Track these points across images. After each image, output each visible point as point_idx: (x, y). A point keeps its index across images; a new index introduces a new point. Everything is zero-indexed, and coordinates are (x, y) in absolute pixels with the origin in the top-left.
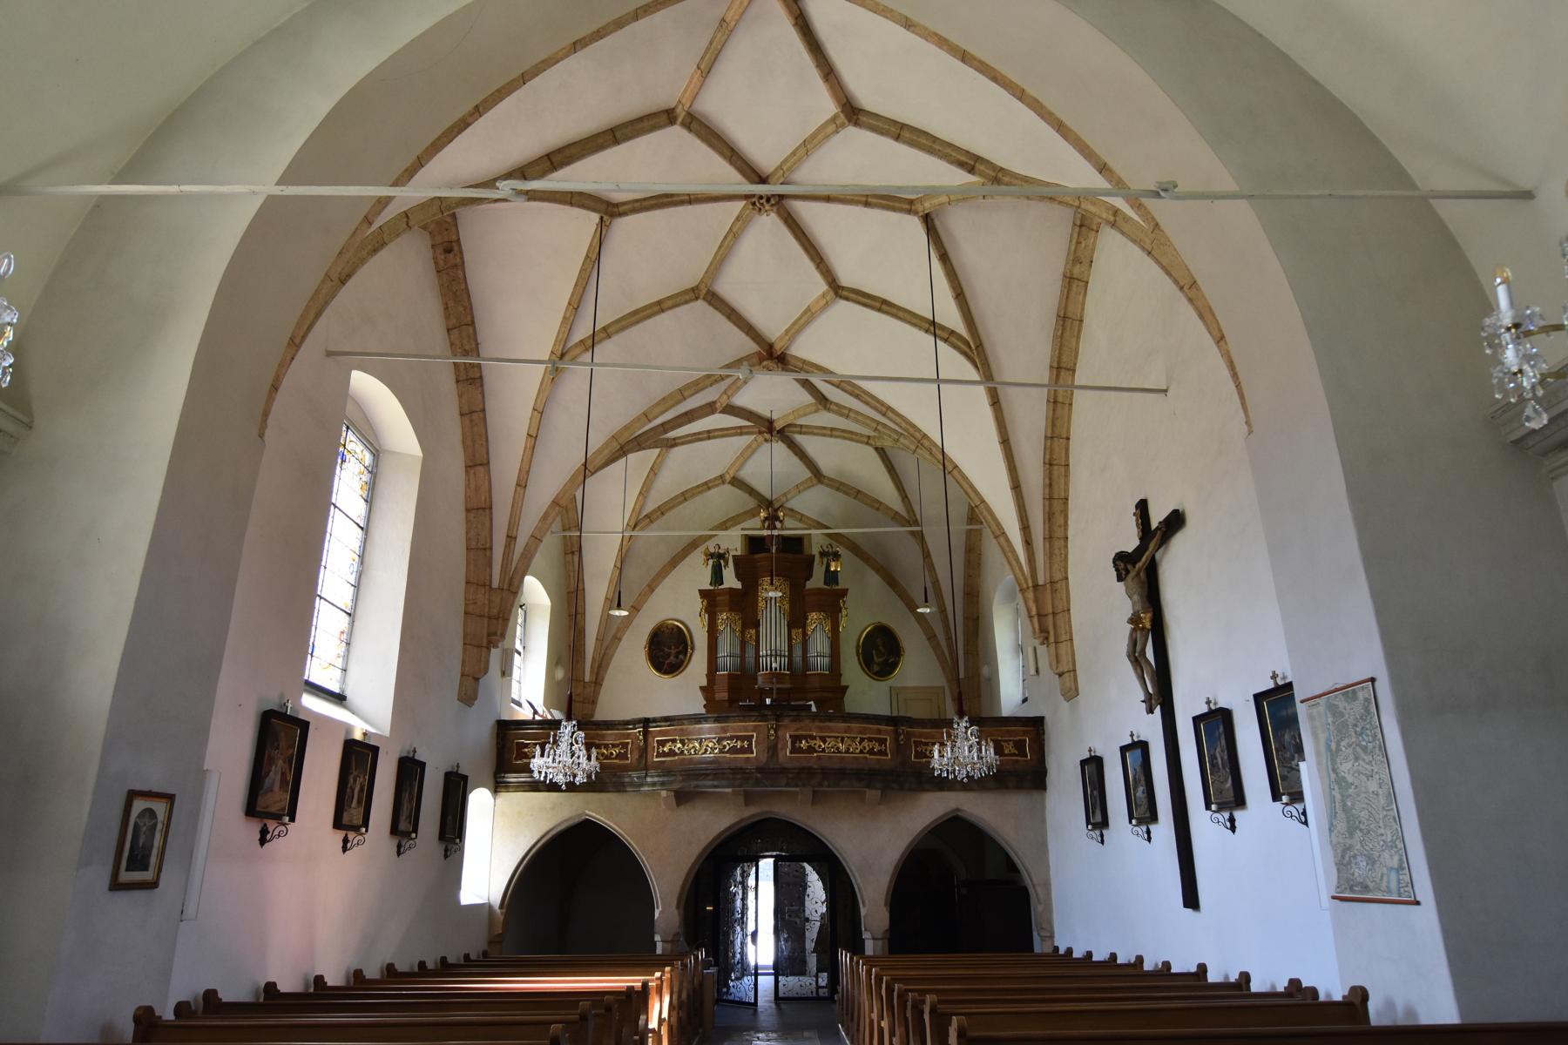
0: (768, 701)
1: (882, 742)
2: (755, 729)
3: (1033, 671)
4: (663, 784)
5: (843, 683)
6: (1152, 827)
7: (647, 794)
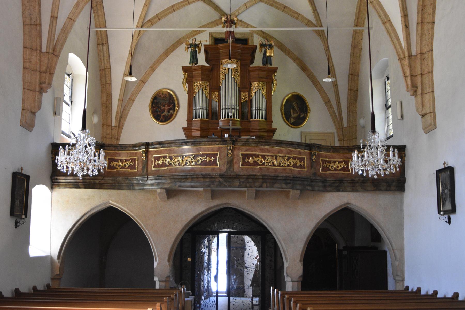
0: (226, 136)
1: (302, 160)
2: (219, 149)
3: (399, 117)
4: (158, 184)
5: (274, 126)
6: (452, 216)
7: (147, 191)
